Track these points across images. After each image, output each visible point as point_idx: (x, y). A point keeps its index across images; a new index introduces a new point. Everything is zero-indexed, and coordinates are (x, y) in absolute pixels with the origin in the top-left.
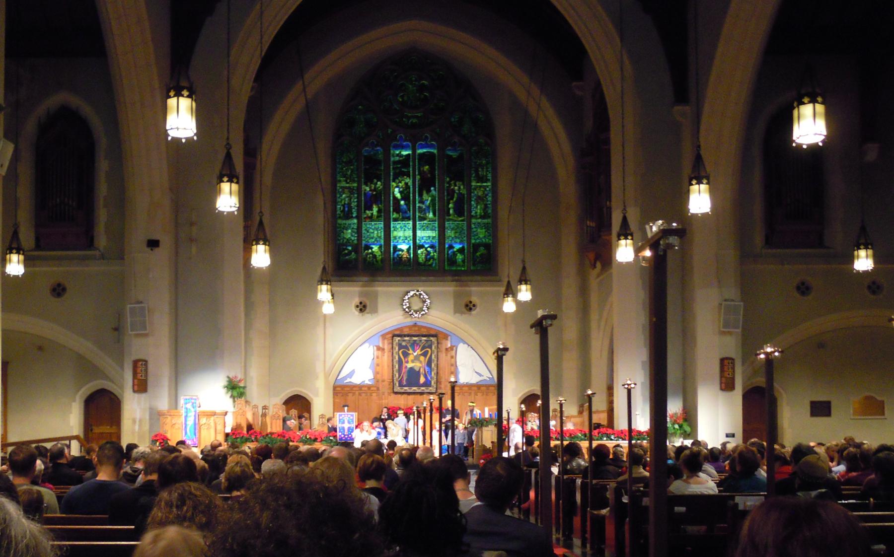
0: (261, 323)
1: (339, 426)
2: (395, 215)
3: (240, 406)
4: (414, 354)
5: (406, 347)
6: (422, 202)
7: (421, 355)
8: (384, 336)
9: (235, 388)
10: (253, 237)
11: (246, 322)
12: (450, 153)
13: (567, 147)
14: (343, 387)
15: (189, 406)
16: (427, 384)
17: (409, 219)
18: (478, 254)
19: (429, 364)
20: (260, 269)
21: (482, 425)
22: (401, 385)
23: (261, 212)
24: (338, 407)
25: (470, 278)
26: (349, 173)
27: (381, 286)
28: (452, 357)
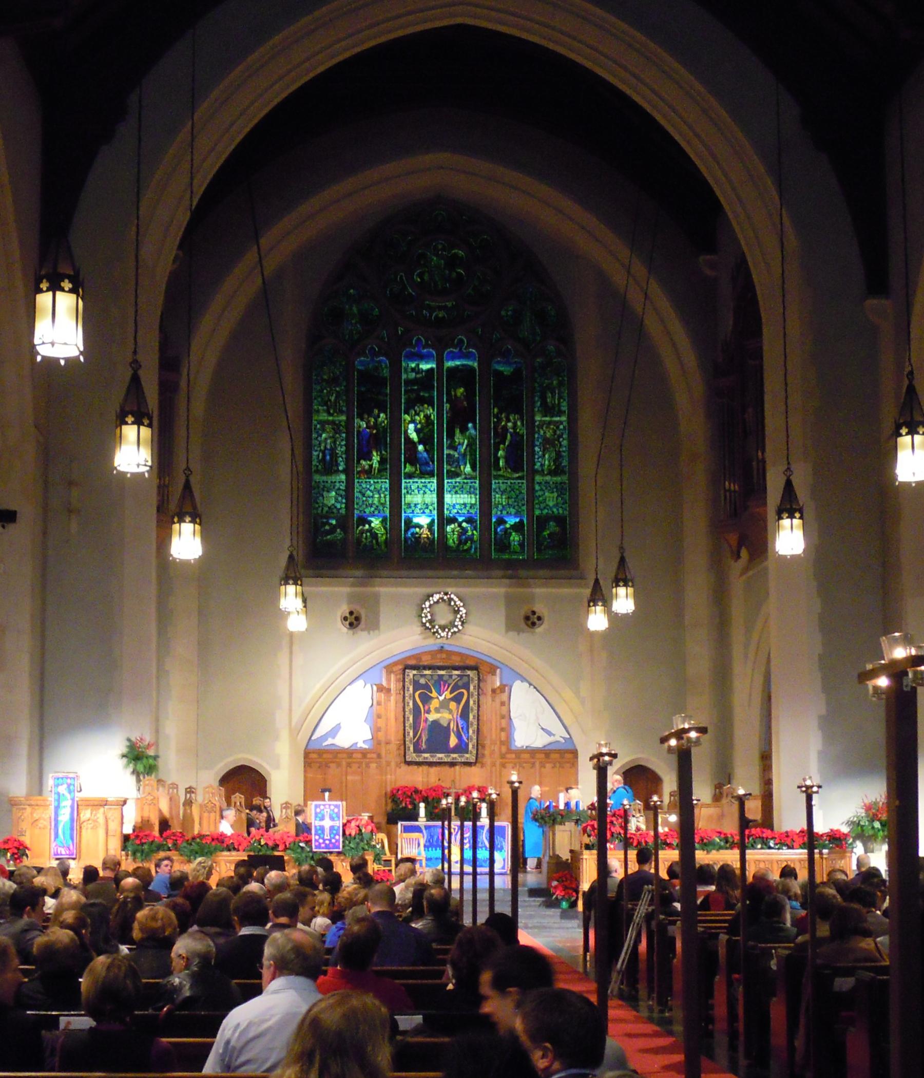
0: (183, 646)
1: (315, 823)
2: (409, 468)
3: (148, 789)
4: (437, 699)
5: (426, 687)
6: (452, 447)
7: (452, 699)
8: (389, 669)
9: (140, 759)
10: (173, 506)
11: (159, 634)
12: (501, 368)
13: (690, 358)
14: (321, 753)
15: (62, 789)
16: (461, 748)
17: (431, 474)
18: (546, 533)
19: (464, 715)
20: (185, 564)
21: (554, 822)
22: (417, 750)
23: (188, 468)
24: (315, 789)
25: (531, 573)
26: (333, 399)
27: (381, 585)
28: (503, 704)
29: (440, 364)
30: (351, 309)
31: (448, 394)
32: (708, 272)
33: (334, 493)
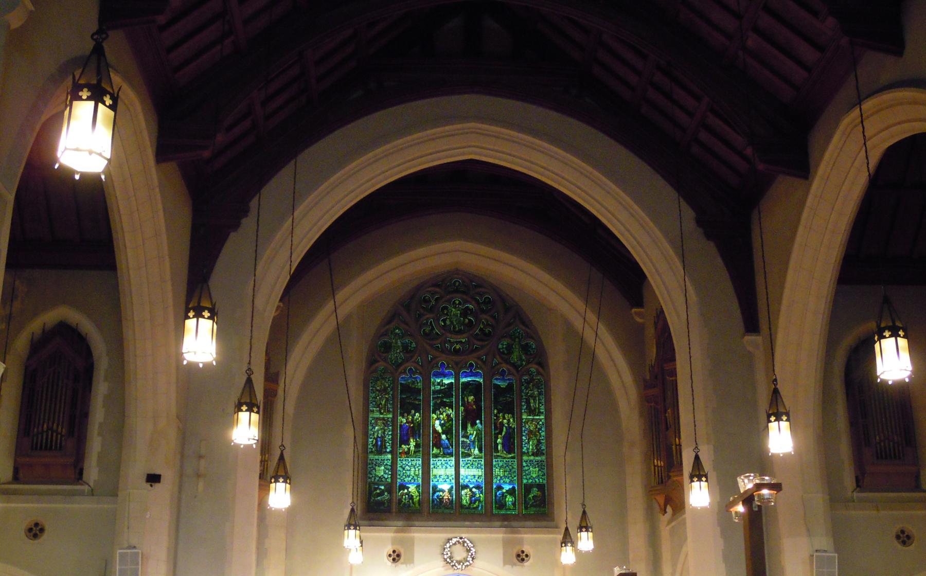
2: (435, 451)
10: (271, 472)
12: (498, 383)
13: (628, 378)
17: (451, 455)
20: (278, 512)
25: (522, 524)
29: (457, 380)
30: (396, 343)
31: (463, 398)
32: (638, 320)
33: (383, 468)
